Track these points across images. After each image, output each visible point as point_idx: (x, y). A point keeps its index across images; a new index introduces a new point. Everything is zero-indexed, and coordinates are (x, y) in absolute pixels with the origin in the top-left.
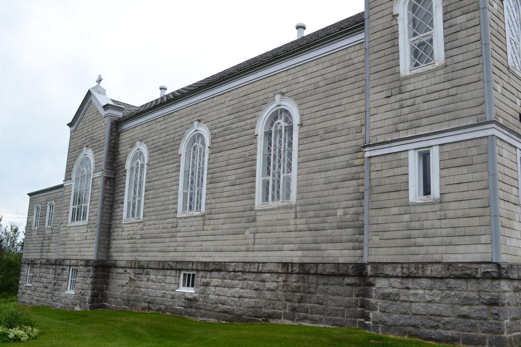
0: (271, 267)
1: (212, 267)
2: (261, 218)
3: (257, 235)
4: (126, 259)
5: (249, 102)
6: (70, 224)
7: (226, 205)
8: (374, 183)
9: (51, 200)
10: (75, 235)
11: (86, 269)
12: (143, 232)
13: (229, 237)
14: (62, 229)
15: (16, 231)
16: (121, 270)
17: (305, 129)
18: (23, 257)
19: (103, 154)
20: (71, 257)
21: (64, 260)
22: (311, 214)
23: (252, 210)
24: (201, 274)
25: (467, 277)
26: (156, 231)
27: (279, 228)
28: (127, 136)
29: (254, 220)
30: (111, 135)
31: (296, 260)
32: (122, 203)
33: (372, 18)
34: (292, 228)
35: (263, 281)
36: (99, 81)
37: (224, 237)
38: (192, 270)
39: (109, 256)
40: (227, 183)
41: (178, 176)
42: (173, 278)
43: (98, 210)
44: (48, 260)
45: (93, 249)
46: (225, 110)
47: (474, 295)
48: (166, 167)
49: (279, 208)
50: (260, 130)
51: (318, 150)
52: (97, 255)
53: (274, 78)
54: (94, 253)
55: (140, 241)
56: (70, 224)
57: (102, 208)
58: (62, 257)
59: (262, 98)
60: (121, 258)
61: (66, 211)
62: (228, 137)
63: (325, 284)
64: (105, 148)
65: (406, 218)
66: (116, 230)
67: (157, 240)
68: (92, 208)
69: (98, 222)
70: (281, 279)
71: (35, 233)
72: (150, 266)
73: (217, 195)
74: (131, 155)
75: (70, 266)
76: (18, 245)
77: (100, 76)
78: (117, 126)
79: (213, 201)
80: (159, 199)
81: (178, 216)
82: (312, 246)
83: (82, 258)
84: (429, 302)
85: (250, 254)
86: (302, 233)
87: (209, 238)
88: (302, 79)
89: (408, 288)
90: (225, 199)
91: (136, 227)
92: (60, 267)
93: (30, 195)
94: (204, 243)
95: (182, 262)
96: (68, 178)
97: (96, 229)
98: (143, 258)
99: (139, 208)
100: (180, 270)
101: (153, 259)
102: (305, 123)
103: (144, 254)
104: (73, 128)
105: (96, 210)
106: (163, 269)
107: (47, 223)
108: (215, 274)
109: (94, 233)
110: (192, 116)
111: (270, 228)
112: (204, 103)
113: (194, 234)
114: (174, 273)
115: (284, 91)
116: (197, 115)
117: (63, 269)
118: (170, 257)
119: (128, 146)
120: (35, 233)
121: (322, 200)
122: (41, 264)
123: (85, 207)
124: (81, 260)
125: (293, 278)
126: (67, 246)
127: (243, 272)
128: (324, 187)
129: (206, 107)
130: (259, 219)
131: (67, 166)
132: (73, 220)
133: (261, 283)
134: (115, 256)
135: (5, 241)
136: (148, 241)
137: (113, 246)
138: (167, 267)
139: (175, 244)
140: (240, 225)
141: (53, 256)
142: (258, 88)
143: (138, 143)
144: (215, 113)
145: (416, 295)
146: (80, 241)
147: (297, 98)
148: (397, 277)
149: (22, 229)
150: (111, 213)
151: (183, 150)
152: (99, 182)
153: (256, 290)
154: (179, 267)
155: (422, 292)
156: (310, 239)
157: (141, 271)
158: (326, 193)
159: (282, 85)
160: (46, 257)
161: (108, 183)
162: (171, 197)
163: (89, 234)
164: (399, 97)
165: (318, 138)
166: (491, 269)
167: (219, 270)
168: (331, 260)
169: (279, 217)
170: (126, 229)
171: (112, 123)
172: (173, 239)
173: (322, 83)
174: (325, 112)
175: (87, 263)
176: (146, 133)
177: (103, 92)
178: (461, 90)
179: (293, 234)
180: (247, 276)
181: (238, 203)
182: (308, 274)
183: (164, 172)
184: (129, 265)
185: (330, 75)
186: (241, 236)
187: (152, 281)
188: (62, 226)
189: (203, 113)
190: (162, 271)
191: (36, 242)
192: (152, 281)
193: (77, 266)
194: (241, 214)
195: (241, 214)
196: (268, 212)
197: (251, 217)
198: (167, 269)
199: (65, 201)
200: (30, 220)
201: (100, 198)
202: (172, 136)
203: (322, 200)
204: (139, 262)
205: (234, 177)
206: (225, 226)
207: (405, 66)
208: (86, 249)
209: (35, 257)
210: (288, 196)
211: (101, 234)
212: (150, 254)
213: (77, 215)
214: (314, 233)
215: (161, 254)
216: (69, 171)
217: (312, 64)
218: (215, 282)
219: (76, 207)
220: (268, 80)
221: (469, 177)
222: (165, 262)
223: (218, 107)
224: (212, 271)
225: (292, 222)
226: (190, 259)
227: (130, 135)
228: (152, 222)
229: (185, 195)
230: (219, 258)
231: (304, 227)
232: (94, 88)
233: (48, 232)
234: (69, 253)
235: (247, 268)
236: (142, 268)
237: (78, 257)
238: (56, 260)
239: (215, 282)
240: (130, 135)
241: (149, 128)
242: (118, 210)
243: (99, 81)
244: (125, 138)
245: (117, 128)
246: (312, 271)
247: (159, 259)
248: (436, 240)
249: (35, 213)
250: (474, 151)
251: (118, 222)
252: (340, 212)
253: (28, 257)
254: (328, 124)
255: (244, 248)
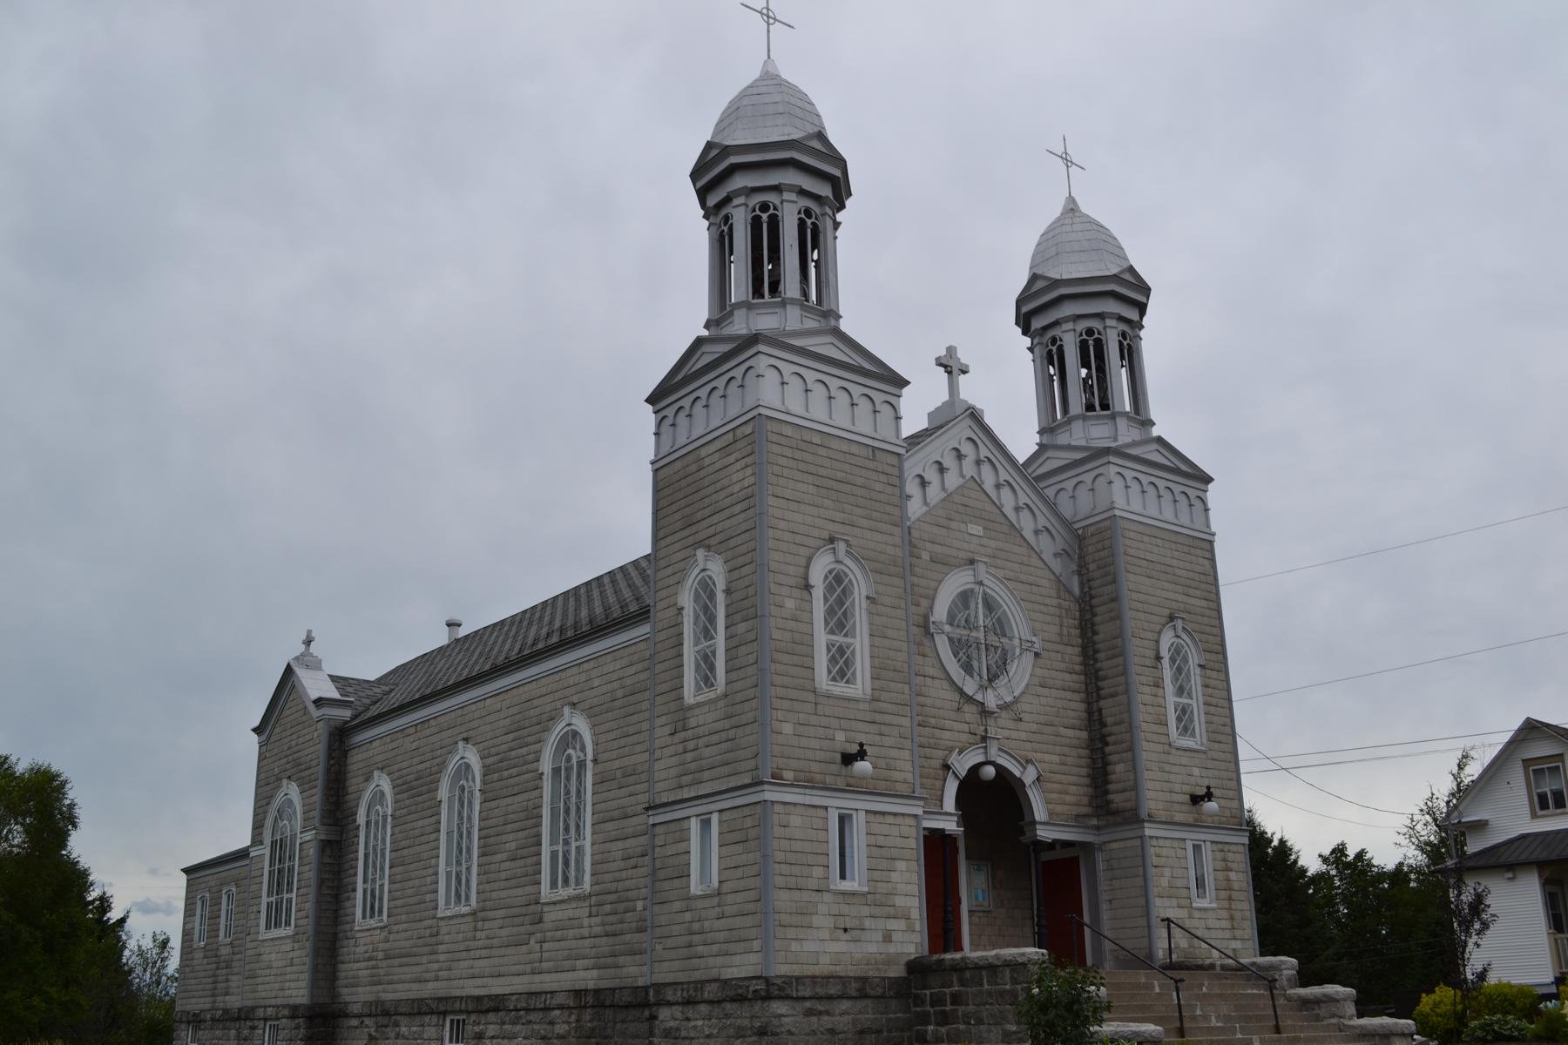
0: (560, 999)
1: (487, 1005)
2: (552, 916)
3: (546, 946)
4: (363, 998)
5: (532, 712)
6: (264, 935)
7: (504, 894)
8: (658, 864)
9: (228, 884)
10: (273, 956)
11: (291, 1023)
12: (388, 945)
13: (511, 950)
14: (249, 945)
15: (164, 944)
16: (355, 1022)
17: (600, 767)
18: (178, 1008)
19: (317, 796)
20: (268, 1002)
21: (254, 1008)
22: (607, 908)
23: (537, 903)
24: (473, 1017)
25: (739, 999)
26: (407, 944)
27: (571, 933)
28: (360, 757)
29: (540, 921)
30: (330, 757)
31: (591, 985)
32: (354, 890)
33: (660, 605)
34: (585, 932)
35: (552, 1023)
36: (308, 642)
37: (502, 951)
38: (461, 1012)
39: (334, 995)
40: (505, 856)
41: (438, 839)
42: (433, 1029)
43: (309, 906)
44: (226, 1011)
45: (304, 984)
46: (501, 723)
47: (746, 1022)
48: (420, 823)
49: (570, 899)
50: (546, 766)
51: (615, 804)
52: (312, 995)
53: (563, 675)
54: (304, 992)
55: (385, 963)
56: (264, 935)
57: (318, 902)
58: (250, 1003)
59: (548, 708)
60: (354, 999)
61: (255, 909)
62: (506, 773)
63: (623, 1021)
64: (320, 783)
65: (688, 916)
66: (345, 942)
67: (413, 960)
68: (301, 901)
69: (310, 930)
70: (573, 1018)
71: (199, 955)
72: (401, 1010)
73: (492, 876)
74: (367, 796)
75: (265, 1020)
76: (171, 978)
77: (309, 632)
78: (340, 738)
79: (487, 887)
80: (410, 883)
81: (440, 915)
82: (610, 960)
83: (285, 1002)
84: (708, 1036)
85: (537, 978)
86: (597, 940)
87: (484, 953)
88: (596, 682)
89: (688, 1019)
90: (502, 884)
91: (379, 936)
92: (249, 1023)
93: (186, 871)
94: (477, 963)
95: (446, 999)
96: (257, 839)
97: (308, 944)
98: (389, 995)
99: (381, 899)
100: (445, 1013)
101: (404, 996)
102: (602, 757)
103: (390, 987)
104: (264, 737)
105: (308, 905)
106: (420, 1013)
107: (222, 933)
108: (491, 1017)
109: (304, 952)
110: (457, 730)
111: (559, 933)
112: (473, 707)
113: (462, 946)
114: (435, 1018)
115: (575, 699)
116: (463, 728)
117: (253, 1028)
118: (430, 990)
119: (361, 779)
120: (199, 955)
121: (621, 886)
122: (213, 1020)
123: (289, 901)
124: (284, 1006)
125: (587, 1015)
126: (259, 980)
127: (527, 1010)
128: (621, 864)
129: (476, 715)
130: (547, 918)
131: (255, 815)
132: (268, 927)
133: (549, 1027)
134: (346, 994)
135: (139, 970)
136: (397, 962)
137: (342, 975)
138: (424, 1009)
139: (436, 966)
140: (522, 929)
141: (234, 1002)
142: (544, 691)
143: (376, 773)
144: (488, 728)
145: (695, 1027)
146: (280, 968)
147: (591, 714)
148: (677, 1003)
149: (176, 943)
150: (336, 911)
151: (443, 793)
152: (311, 852)
153: (543, 1038)
154: (442, 1008)
155: (700, 1023)
156: (606, 950)
157: (385, 1020)
158: (624, 874)
159: (572, 690)
160: (221, 1005)
161: (328, 852)
162: (429, 880)
163: (296, 954)
164: (683, 735)
165: (614, 784)
166: (761, 986)
167: (496, 1010)
168: (628, 982)
169: (570, 913)
170: (362, 941)
171: (331, 734)
172: (433, 957)
173: (619, 693)
174: (622, 742)
175: (294, 1012)
176: (390, 755)
177: (314, 665)
178: (740, 732)
179: (587, 942)
180: (533, 1016)
181: (520, 891)
182: (604, 1006)
183: (417, 832)
184: (366, 1010)
185: (628, 681)
186: (524, 949)
187: (404, 1037)
188: (249, 938)
189: (472, 725)
190: (418, 1018)
191: (202, 974)
192: (404, 1037)
193: (277, 1019)
194: (524, 910)
195: (524, 910)
196: (558, 907)
197: (533, 912)
198: (426, 1014)
199: (254, 887)
200: (189, 926)
201: (313, 882)
202: (427, 764)
203: (621, 886)
204: (383, 1002)
205: (513, 845)
206: (504, 932)
207: (689, 694)
208: (293, 985)
209: (200, 1007)
210: (578, 882)
211: (316, 952)
212: (400, 987)
213: (277, 916)
214: (611, 940)
215: (415, 986)
216: (258, 826)
217: (609, 658)
218: (492, 1030)
219: (273, 899)
220: (556, 677)
221: (743, 859)
222: (422, 1000)
223: (493, 717)
224: (487, 1011)
225: (586, 922)
226: (458, 993)
227: (364, 756)
228: (402, 927)
229: (449, 874)
230: (497, 987)
231: (597, 930)
232: (297, 658)
233: (225, 951)
234: (263, 994)
235: (532, 1003)
236: (386, 1013)
237: (279, 1002)
238: (240, 1010)
239: (492, 1030)
240: (364, 756)
241: (394, 745)
242: (348, 904)
243: (308, 642)
244: (356, 760)
245: (342, 742)
246: (608, 1002)
247: (412, 995)
248: (715, 948)
249: (198, 912)
250: (749, 822)
251: (348, 927)
252: (639, 905)
253: (188, 1008)
254: (626, 761)
255: (528, 968)
